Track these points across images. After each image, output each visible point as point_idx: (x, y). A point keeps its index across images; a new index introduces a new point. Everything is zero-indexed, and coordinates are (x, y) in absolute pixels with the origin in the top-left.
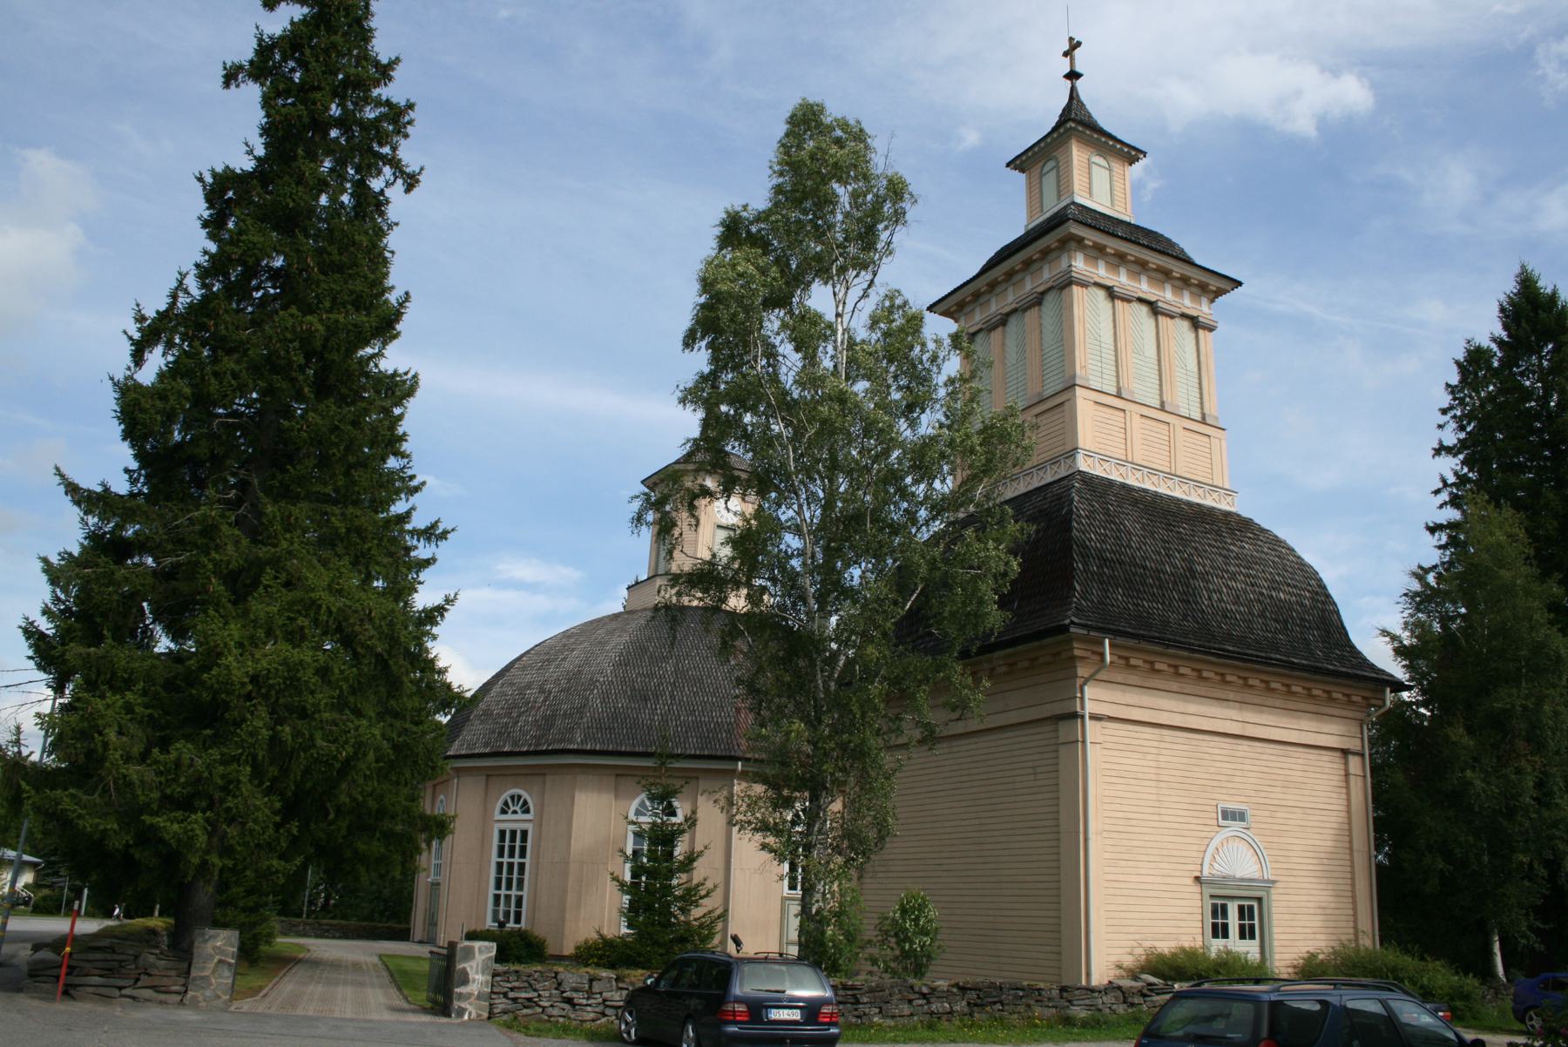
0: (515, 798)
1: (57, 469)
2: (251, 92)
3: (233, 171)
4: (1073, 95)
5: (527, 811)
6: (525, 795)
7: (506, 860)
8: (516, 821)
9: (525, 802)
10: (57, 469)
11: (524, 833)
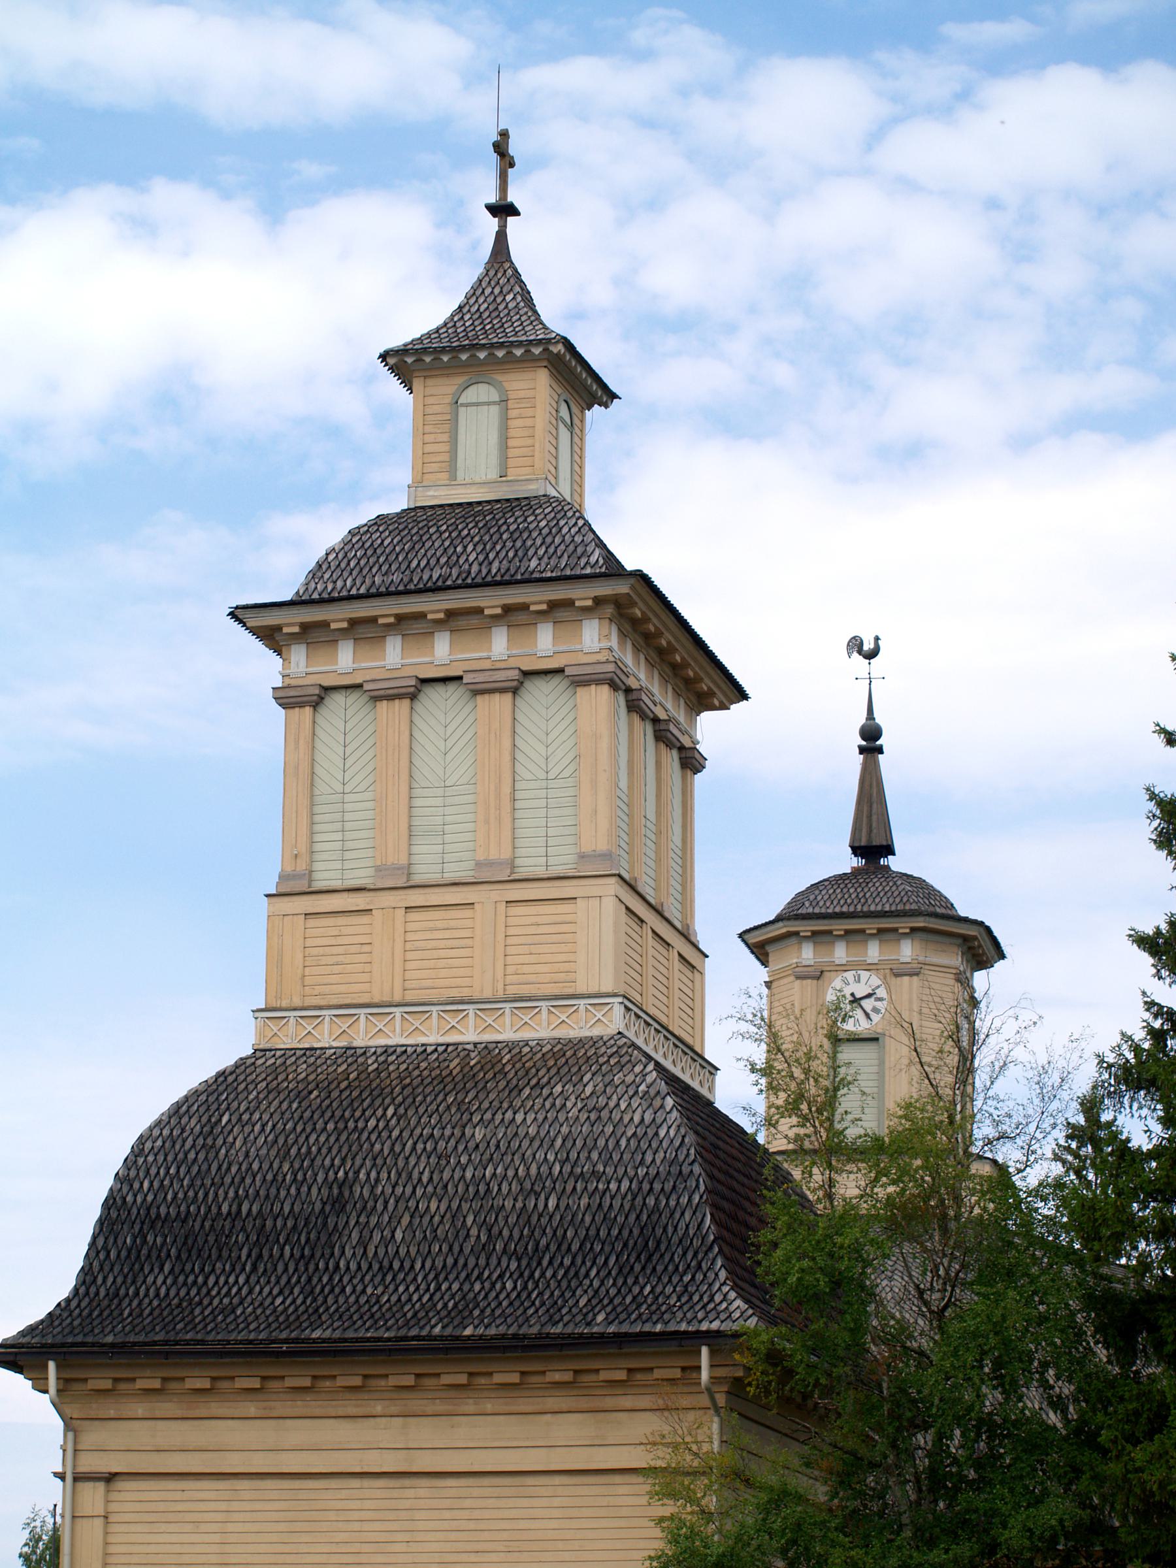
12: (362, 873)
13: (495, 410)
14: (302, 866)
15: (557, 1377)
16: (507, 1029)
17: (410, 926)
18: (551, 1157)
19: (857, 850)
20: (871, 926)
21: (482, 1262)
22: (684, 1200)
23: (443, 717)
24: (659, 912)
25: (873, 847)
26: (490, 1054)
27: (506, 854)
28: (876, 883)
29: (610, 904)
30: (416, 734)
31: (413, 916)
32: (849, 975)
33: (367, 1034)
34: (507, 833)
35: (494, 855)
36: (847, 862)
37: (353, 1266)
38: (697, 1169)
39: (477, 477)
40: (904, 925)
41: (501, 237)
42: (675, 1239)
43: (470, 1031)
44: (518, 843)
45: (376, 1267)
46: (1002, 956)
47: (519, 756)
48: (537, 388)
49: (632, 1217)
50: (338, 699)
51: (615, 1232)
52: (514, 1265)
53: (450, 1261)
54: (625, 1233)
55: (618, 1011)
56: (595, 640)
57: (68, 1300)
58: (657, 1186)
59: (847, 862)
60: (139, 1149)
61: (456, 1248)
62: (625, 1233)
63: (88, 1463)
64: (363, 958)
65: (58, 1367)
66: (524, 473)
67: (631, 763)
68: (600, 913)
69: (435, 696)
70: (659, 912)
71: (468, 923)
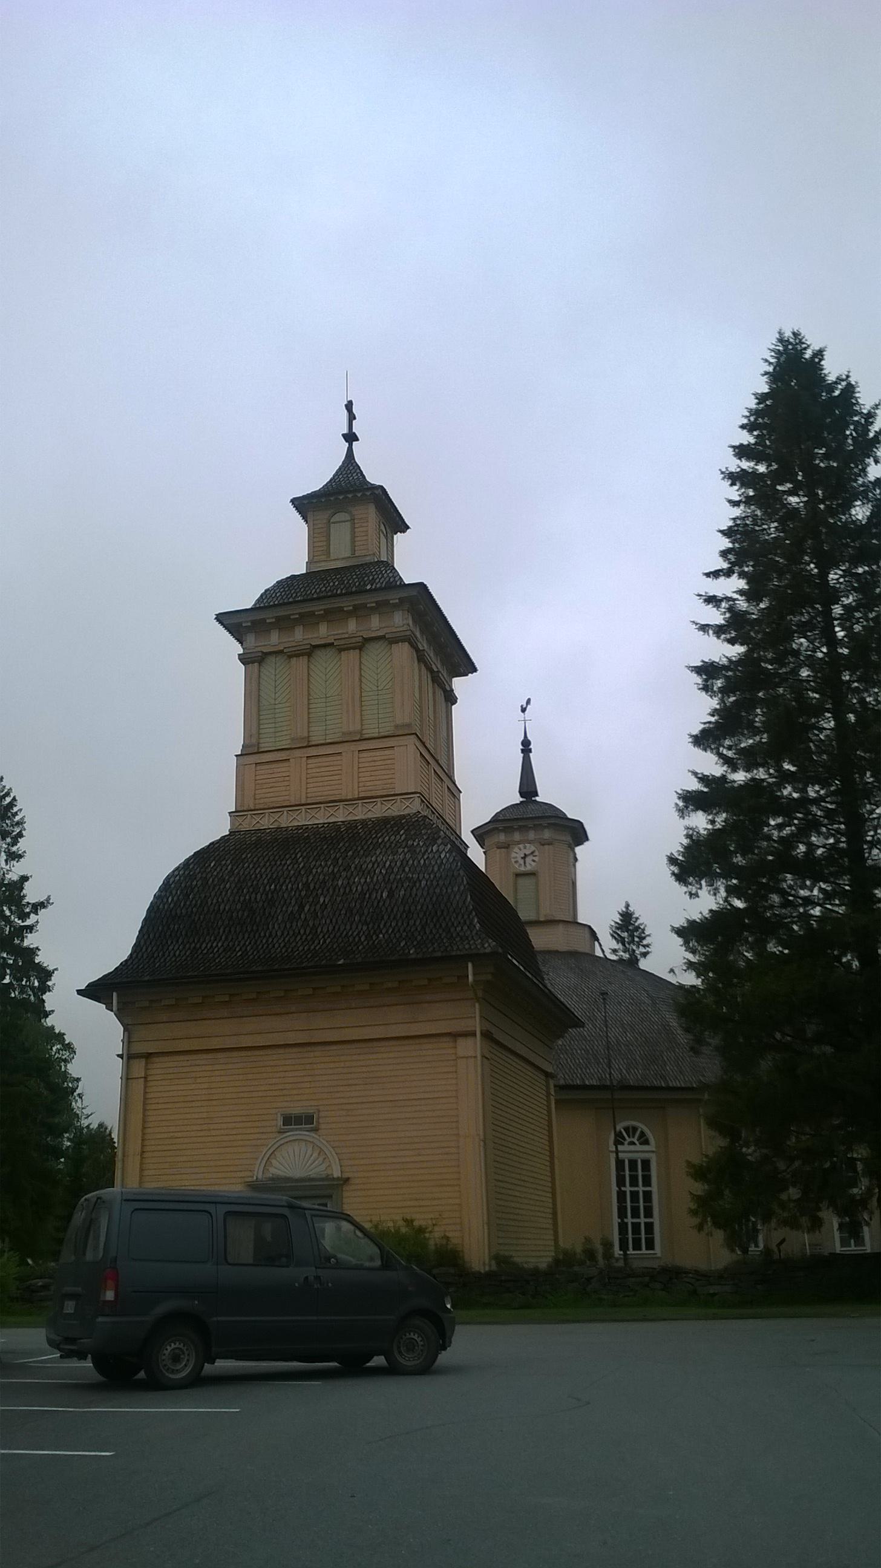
0: (631, 1131)
1: (708, 575)
2: (48, 1009)
3: (694, 921)
4: (350, 454)
5: (646, 1142)
6: (642, 1127)
7: (642, 1220)
8: (631, 1150)
9: (643, 1134)
10: (708, 575)
11: (646, 1164)
12: (284, 743)
13: (348, 524)
14: (254, 741)
15: (390, 985)
16: (360, 813)
17: (310, 766)
18: (383, 871)
19: (522, 794)
20: (530, 824)
21: (348, 927)
22: (456, 889)
23: (325, 666)
24: (437, 761)
25: (528, 787)
26: (351, 826)
27: (358, 727)
28: (531, 807)
29: (412, 749)
30: (311, 673)
31: (310, 761)
32: (521, 846)
33: (287, 820)
34: (358, 717)
35: (351, 729)
36: (517, 799)
37: (279, 933)
38: (462, 873)
39: (341, 554)
40: (544, 822)
41: (350, 451)
42: (451, 909)
43: (341, 816)
44: (365, 722)
45: (291, 933)
46: (587, 839)
47: (364, 680)
48: (370, 514)
49: (428, 900)
50: (271, 660)
51: (419, 907)
52: (365, 928)
53: (331, 928)
54: (425, 908)
55: (417, 801)
56: (400, 621)
57: (126, 961)
58: (441, 883)
59: (517, 799)
60: (167, 886)
61: (334, 920)
62: (425, 908)
63: (139, 1048)
64: (286, 783)
65: (118, 996)
66: (364, 552)
67: (420, 687)
68: (407, 753)
69: (320, 654)
70: (437, 761)
71: (339, 763)
